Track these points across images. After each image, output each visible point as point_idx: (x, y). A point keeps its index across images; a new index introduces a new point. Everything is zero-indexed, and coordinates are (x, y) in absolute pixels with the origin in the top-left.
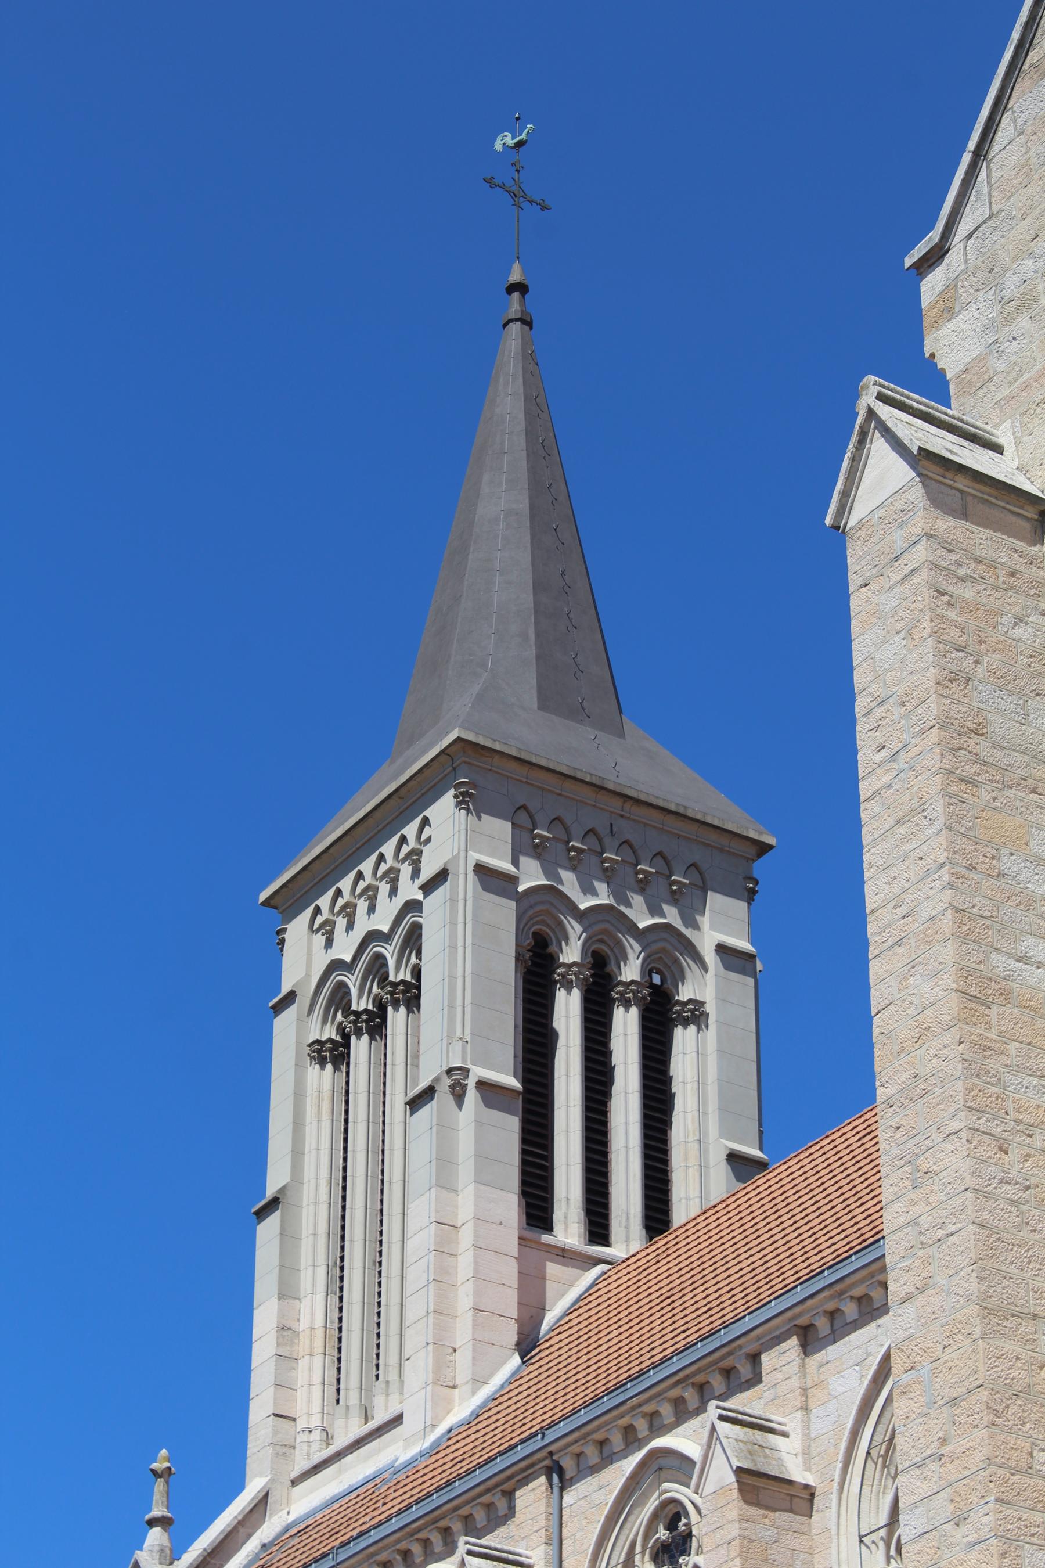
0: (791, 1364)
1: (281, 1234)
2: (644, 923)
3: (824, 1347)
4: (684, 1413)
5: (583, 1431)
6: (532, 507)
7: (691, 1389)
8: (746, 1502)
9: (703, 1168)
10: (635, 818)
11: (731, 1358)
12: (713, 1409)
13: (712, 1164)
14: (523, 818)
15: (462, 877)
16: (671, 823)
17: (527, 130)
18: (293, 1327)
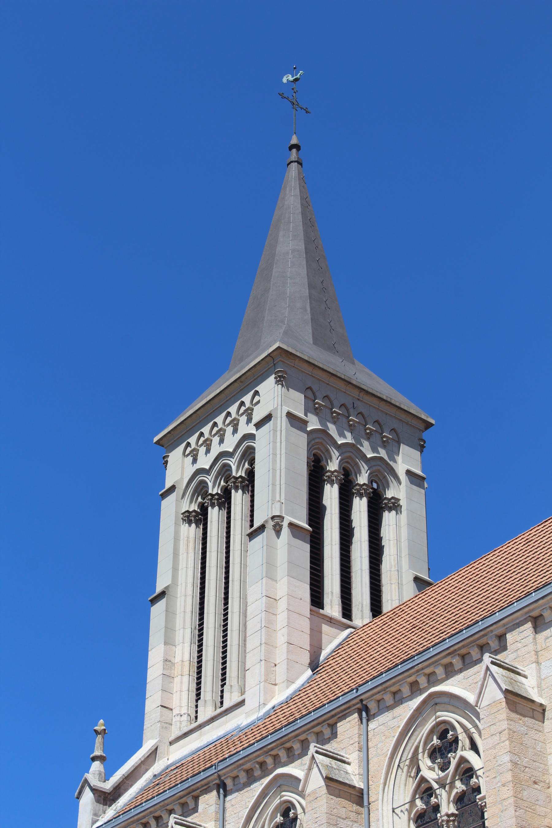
0: (527, 638)
1: (166, 611)
2: (370, 455)
4: (452, 672)
5: (384, 686)
6: (306, 248)
7: (457, 658)
8: (510, 710)
9: (400, 585)
10: (365, 401)
11: (485, 638)
12: (487, 658)
13: (404, 583)
15: (279, 419)
16: (382, 405)
17: (300, 74)
18: (171, 660)
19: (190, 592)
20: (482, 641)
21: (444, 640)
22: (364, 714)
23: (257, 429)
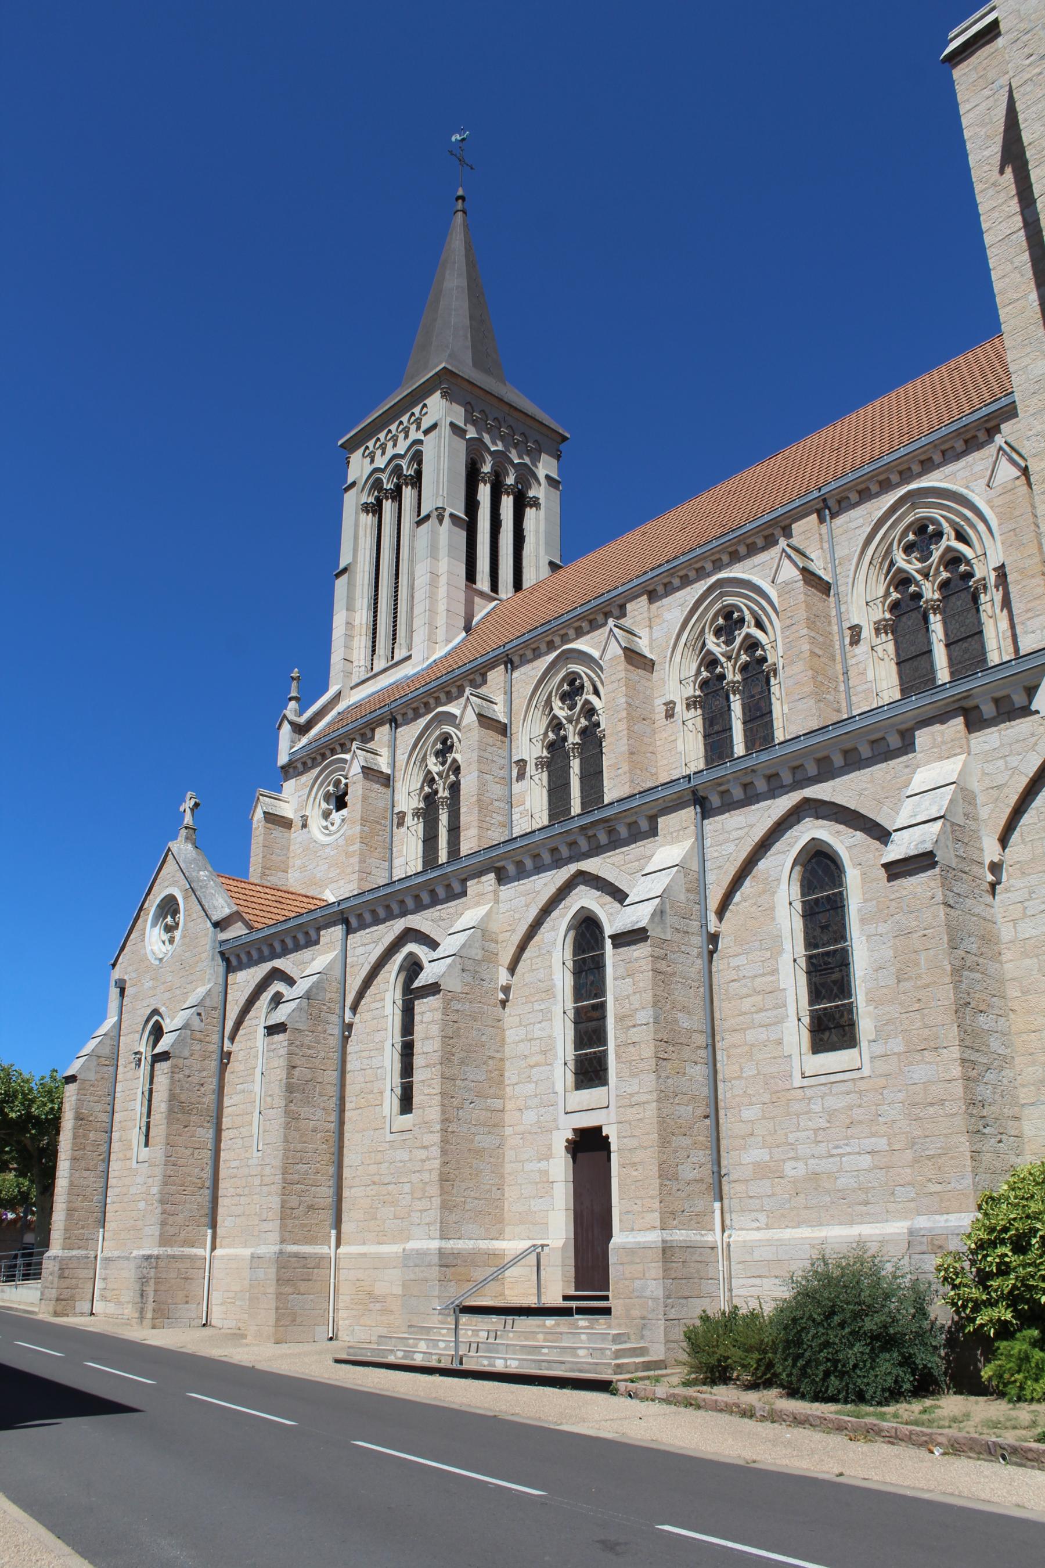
1: (348, 583)
3: (661, 599)
9: (537, 568)
12: (611, 622)
14: (469, 407)
19: (367, 568)
20: (607, 609)
21: (576, 608)
22: (509, 665)
23: (425, 436)
